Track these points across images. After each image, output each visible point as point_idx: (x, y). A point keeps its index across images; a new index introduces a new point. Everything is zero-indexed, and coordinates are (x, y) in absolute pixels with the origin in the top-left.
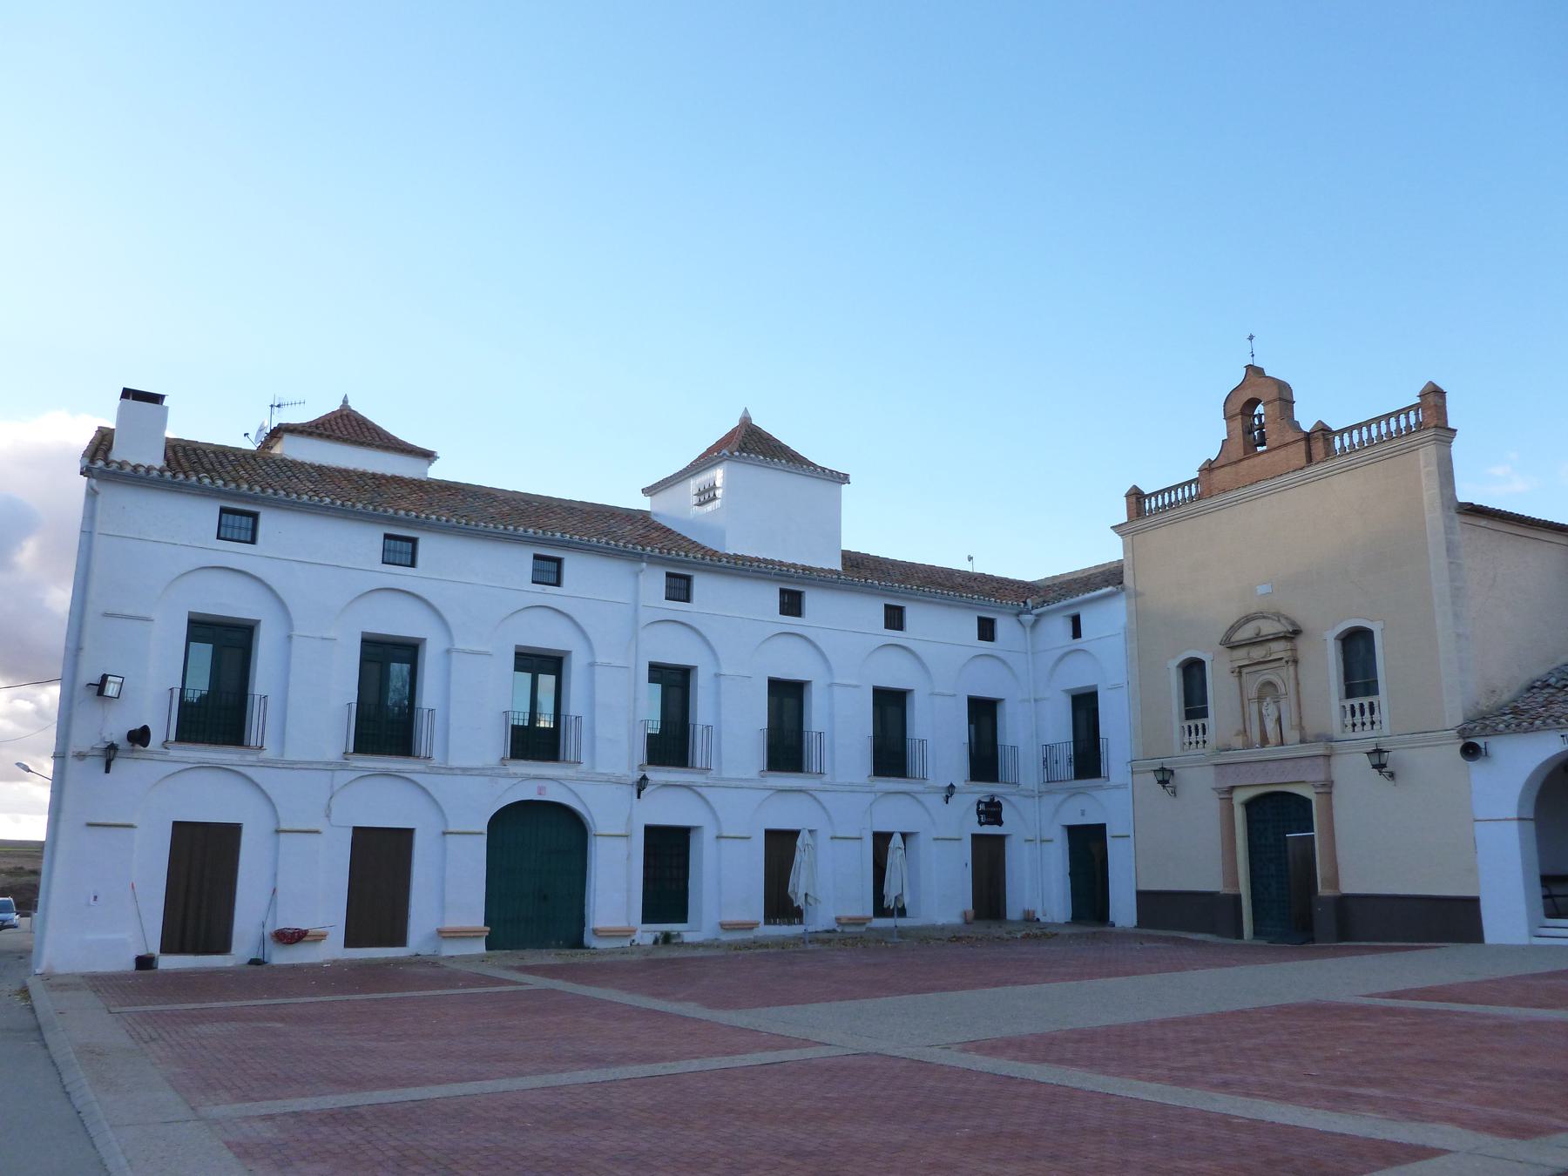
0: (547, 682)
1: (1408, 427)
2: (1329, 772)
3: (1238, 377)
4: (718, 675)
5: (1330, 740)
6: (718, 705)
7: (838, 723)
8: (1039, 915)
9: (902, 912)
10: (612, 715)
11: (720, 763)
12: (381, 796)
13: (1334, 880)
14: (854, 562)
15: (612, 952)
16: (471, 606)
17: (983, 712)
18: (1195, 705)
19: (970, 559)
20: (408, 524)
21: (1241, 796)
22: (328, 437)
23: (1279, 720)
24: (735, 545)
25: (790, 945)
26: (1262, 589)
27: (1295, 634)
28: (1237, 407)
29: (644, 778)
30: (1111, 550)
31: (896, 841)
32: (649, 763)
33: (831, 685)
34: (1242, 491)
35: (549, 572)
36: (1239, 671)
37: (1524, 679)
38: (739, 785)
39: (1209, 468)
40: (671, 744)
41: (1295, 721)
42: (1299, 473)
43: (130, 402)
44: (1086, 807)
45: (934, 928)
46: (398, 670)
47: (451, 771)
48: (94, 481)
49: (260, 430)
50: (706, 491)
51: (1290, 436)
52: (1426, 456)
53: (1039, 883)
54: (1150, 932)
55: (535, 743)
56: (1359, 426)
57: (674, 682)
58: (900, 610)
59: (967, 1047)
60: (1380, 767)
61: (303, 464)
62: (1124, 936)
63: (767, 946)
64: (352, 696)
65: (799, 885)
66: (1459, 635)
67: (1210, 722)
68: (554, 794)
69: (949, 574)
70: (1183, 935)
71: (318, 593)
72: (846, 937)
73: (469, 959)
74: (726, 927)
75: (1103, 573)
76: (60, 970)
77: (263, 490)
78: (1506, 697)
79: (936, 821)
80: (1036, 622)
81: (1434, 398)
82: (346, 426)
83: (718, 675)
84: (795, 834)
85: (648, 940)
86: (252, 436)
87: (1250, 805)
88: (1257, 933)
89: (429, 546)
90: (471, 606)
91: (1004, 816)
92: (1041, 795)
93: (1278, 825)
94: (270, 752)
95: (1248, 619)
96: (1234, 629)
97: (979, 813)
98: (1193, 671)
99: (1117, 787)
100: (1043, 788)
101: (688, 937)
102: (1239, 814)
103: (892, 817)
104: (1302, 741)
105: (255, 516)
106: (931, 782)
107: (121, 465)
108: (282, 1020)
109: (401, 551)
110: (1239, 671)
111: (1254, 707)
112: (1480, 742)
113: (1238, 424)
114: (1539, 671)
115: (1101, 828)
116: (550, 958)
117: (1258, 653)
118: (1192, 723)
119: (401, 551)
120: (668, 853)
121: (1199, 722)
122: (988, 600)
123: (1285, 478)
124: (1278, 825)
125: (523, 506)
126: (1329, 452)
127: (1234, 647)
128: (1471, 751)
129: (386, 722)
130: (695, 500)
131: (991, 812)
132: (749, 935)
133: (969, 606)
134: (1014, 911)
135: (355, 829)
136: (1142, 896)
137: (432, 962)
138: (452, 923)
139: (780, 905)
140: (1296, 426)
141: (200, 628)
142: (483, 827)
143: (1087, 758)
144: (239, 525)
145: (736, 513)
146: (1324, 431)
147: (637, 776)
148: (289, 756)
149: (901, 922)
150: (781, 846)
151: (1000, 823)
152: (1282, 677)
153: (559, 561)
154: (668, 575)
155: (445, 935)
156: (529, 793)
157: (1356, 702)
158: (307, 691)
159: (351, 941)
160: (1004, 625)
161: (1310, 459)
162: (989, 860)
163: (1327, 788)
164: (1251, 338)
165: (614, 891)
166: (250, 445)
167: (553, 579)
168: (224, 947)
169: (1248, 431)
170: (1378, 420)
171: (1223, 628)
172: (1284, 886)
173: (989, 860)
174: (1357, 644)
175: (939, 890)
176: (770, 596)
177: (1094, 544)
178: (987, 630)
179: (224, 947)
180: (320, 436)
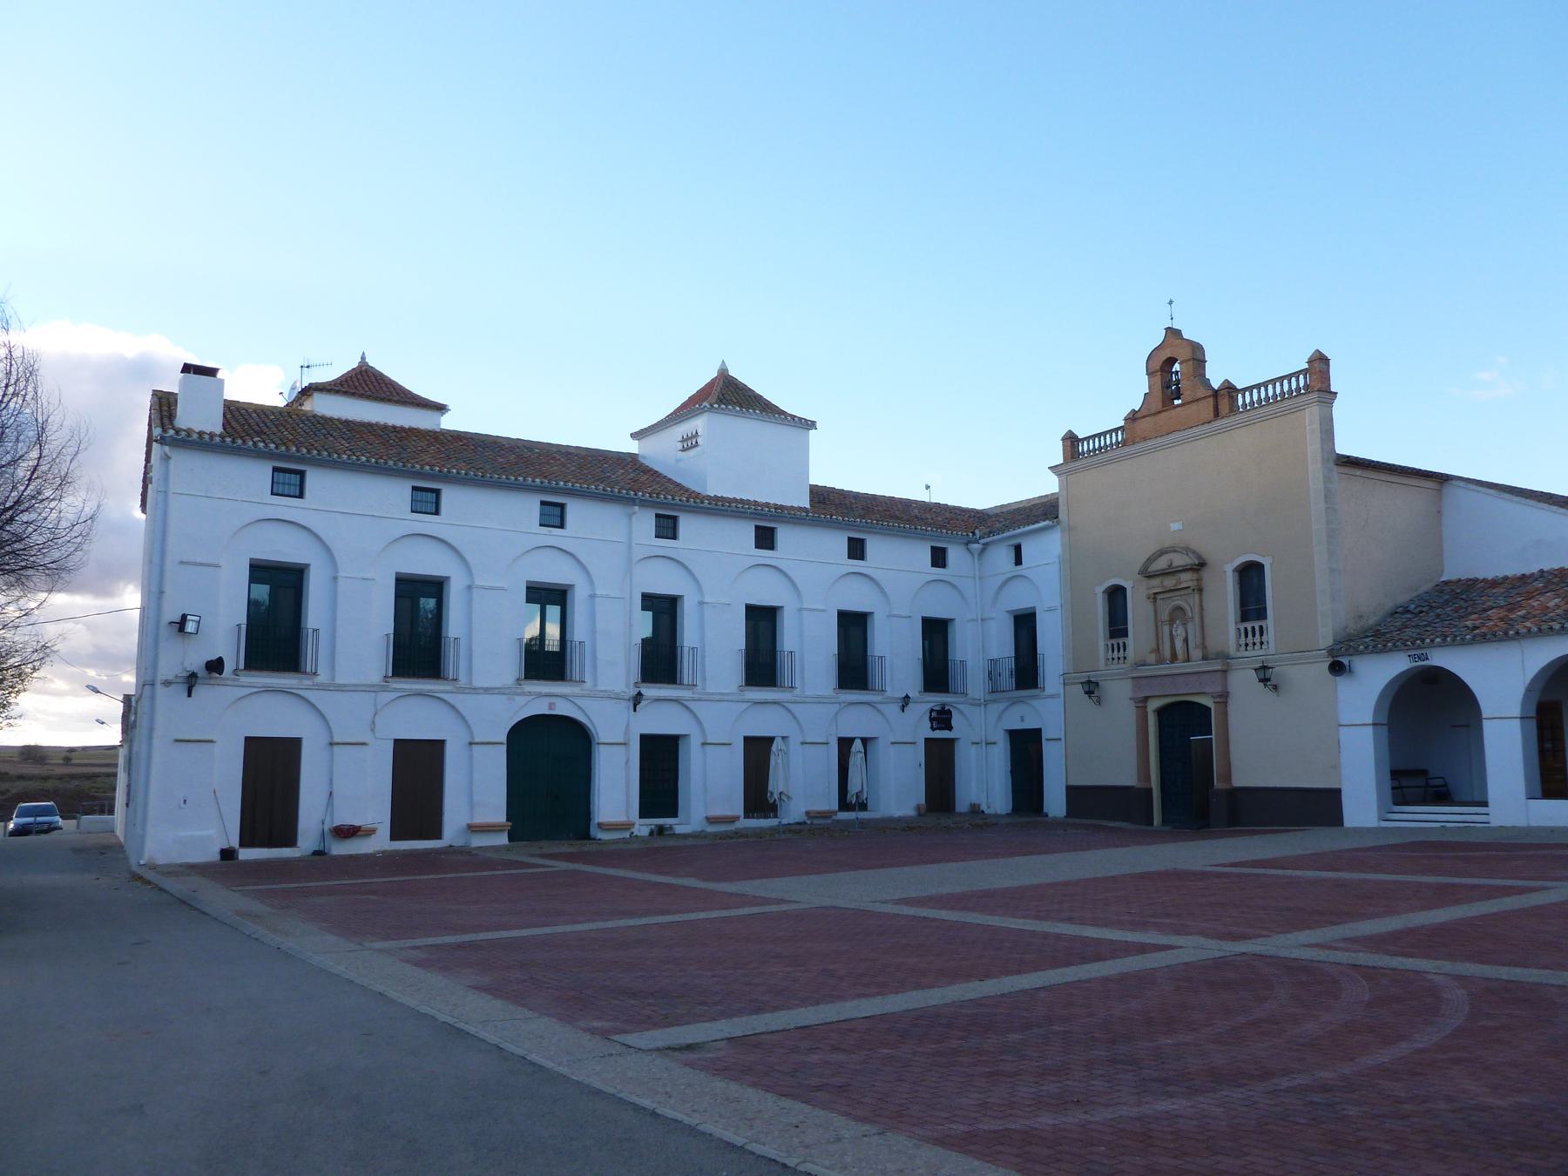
0: (553, 611)
1: (1298, 389)
2: (1225, 685)
3: (1159, 338)
4: (701, 603)
5: (1228, 657)
6: (702, 626)
7: (809, 644)
8: (984, 807)
9: (863, 806)
10: (611, 637)
11: (704, 680)
12: (416, 714)
13: (1227, 776)
14: (821, 496)
15: (615, 842)
16: (488, 549)
17: (936, 631)
18: (1117, 627)
19: (928, 487)
20: (432, 477)
21: (1154, 705)
22: (353, 394)
23: (1186, 640)
24: (715, 488)
25: (765, 831)
26: (1175, 526)
27: (1200, 566)
28: (1157, 364)
29: (640, 694)
30: (1049, 485)
31: (858, 745)
32: (644, 681)
33: (800, 610)
34: (1160, 440)
35: (554, 516)
36: (1154, 598)
37: (1389, 605)
38: (720, 698)
39: (1133, 417)
40: (661, 660)
41: (1198, 639)
42: (1207, 426)
43: (192, 376)
44: (1024, 716)
45: (891, 820)
46: (429, 603)
47: (474, 690)
48: (167, 448)
49: (293, 388)
50: (688, 438)
51: (1201, 392)
52: (1311, 414)
53: (984, 781)
54: (1077, 821)
55: (544, 663)
56: (1258, 386)
57: (664, 608)
58: (862, 542)
59: (899, 902)
60: (1265, 680)
61: (331, 419)
62: (1056, 823)
63: (746, 836)
64: (389, 626)
65: (777, 783)
66: (1332, 570)
67: (1130, 641)
68: (563, 709)
69: (907, 504)
70: (1104, 823)
71: (357, 537)
72: (815, 828)
73: (496, 849)
74: (711, 820)
75: (1044, 504)
76: (160, 862)
77: (309, 452)
78: (1372, 621)
79: (895, 729)
80: (983, 550)
81: (1319, 363)
82: (365, 382)
83: (701, 603)
84: (771, 740)
85: (645, 832)
86: (286, 395)
87: (1161, 712)
88: (1165, 821)
89: (451, 496)
90: (488, 549)
91: (953, 723)
92: (986, 703)
93: (1184, 729)
94: (322, 678)
95: (1162, 553)
96: (1150, 560)
97: (931, 720)
98: (1116, 596)
99: (1052, 696)
100: (988, 697)
101: (679, 830)
102: (1152, 721)
103: (856, 723)
104: (1205, 658)
105: (302, 474)
106: (888, 694)
107: (189, 432)
108: (374, 893)
109: (426, 501)
110: (1154, 598)
111: (1166, 629)
112: (1345, 660)
113: (1158, 379)
114: (1402, 599)
115: (1037, 733)
116: (565, 847)
117: (1169, 582)
118: (1114, 641)
119: (426, 501)
120: (660, 760)
121: (1121, 641)
122: (941, 528)
123: (1195, 430)
124: (1184, 729)
125: (527, 454)
126: (1233, 408)
127: (1149, 577)
128: (1337, 668)
129: (419, 646)
130: (680, 446)
131: (942, 718)
132: (732, 827)
133: (922, 537)
134: (962, 805)
135: (396, 741)
136: (1071, 790)
137: (465, 851)
138: (480, 819)
139: (758, 797)
140: (1207, 383)
141: (260, 571)
142: (503, 737)
143: (1026, 672)
144: (290, 483)
145: (725, 460)
146: (1229, 389)
147: (634, 692)
148: (340, 680)
149: (863, 815)
150: (758, 751)
151: (950, 728)
152: (1189, 603)
153: (562, 506)
154: (657, 516)
155: (473, 829)
156: (540, 708)
157: (1249, 625)
158: (351, 623)
159: (394, 836)
160: (955, 554)
161: (1217, 414)
162: (940, 761)
163: (1223, 698)
164: (1171, 303)
165: (615, 792)
166: (281, 403)
167: (557, 521)
168: (291, 841)
169: (1166, 385)
170: (1273, 382)
171: (1138, 566)
172: (1187, 777)
173: (940, 761)
174: (1250, 575)
175: (897, 788)
176: (745, 532)
177: (1036, 480)
178: (939, 558)
179: (291, 841)
180: (346, 393)
